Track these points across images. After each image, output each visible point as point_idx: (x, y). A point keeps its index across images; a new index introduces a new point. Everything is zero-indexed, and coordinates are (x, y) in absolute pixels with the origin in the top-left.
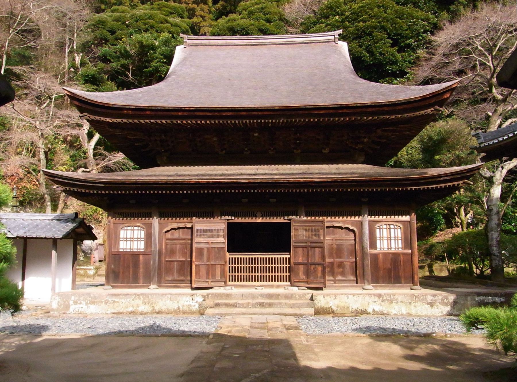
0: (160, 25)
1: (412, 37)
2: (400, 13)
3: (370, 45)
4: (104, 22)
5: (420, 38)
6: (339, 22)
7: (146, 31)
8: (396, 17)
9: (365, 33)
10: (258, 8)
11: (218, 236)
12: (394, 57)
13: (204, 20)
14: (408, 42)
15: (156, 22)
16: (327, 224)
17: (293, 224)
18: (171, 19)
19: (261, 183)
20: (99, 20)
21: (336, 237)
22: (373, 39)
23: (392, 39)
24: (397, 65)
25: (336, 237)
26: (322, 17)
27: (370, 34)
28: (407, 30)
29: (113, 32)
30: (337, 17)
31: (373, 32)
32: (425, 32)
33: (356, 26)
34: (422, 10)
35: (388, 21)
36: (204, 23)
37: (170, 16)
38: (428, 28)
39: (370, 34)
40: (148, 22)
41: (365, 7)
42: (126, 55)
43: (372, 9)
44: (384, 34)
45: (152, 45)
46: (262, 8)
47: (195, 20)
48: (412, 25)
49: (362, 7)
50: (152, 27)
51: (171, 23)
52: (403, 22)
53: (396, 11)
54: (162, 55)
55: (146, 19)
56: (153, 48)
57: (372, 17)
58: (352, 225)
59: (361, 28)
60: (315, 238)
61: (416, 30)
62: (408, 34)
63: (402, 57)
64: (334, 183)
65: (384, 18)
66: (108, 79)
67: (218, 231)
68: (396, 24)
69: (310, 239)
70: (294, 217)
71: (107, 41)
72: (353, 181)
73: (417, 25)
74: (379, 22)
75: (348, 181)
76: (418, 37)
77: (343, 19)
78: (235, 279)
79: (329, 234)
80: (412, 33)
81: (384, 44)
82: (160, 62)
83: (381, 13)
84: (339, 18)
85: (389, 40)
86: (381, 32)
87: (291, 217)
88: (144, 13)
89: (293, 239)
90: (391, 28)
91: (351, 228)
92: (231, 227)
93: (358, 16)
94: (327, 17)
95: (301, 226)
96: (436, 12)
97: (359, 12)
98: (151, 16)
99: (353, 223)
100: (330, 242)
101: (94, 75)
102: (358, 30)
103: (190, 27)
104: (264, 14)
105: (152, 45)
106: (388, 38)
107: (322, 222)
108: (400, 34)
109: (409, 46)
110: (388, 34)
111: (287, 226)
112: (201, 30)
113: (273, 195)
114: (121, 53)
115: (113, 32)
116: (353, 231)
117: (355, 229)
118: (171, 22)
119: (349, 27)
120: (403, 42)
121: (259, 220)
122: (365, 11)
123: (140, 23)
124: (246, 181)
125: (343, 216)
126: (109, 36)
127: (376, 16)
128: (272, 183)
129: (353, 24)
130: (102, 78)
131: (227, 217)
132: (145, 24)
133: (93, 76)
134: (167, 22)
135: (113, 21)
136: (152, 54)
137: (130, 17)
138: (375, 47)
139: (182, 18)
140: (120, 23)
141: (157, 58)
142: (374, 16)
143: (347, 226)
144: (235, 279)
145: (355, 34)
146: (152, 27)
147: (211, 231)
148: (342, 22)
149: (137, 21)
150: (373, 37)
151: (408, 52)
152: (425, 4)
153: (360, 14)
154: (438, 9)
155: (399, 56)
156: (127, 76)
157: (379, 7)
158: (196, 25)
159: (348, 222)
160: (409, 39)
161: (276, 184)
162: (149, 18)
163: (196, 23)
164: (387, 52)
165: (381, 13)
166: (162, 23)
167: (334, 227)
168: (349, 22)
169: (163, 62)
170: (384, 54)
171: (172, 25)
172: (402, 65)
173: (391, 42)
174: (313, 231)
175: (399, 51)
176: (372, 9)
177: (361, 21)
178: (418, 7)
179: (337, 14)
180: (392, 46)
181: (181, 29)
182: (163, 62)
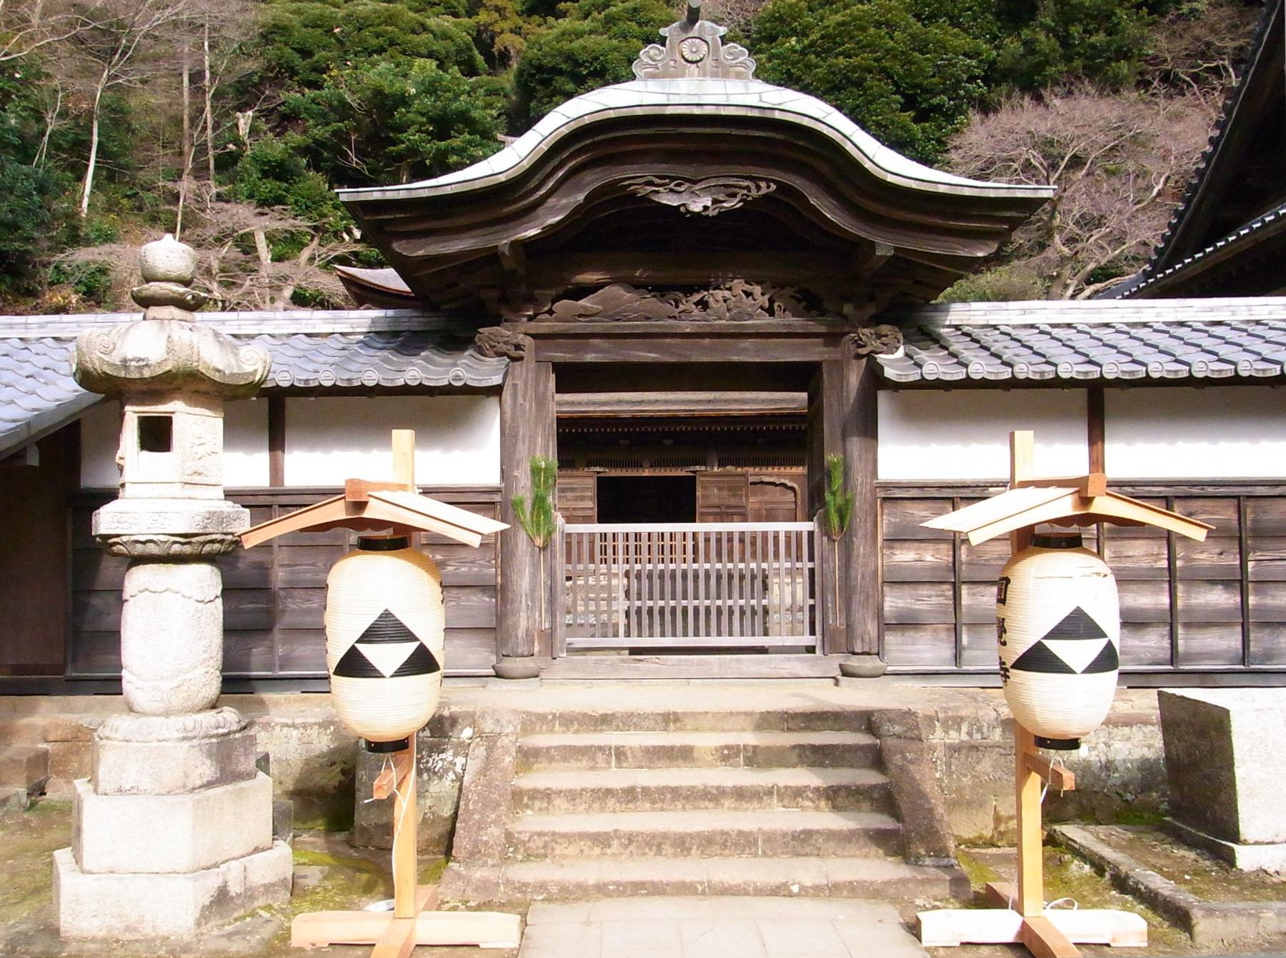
0: (410, 37)
1: (943, 92)
2: (922, 40)
3: (858, 106)
4: (285, 28)
5: (962, 92)
6: (796, 51)
7: (381, 50)
8: (913, 49)
9: (849, 80)
10: (626, 11)
11: (583, 498)
12: (908, 131)
13: (504, 18)
14: (935, 101)
15: (401, 29)
16: (751, 479)
17: (699, 479)
18: (432, 22)
19: (651, 418)
20: (274, 25)
21: (766, 498)
22: (865, 94)
23: (903, 95)
24: (913, 147)
25: (766, 498)
26: (763, 39)
27: (859, 84)
28: (933, 76)
29: (306, 53)
30: (793, 41)
31: (865, 80)
32: (972, 79)
33: (830, 66)
34: (965, 30)
35: (895, 57)
36: (506, 25)
37: (429, 12)
38: (977, 72)
39: (859, 84)
40: (386, 32)
41: (849, 23)
42: (343, 110)
43: (864, 29)
44: (887, 84)
45: (403, 94)
46: (635, 10)
47: (483, 17)
48: (945, 66)
49: (843, 24)
50: (392, 43)
51: (432, 32)
52: (927, 59)
53: (913, 37)
54: (423, 115)
55: (379, 25)
56: (403, 100)
57: (863, 47)
58: (791, 480)
59: (840, 70)
60: (732, 501)
61: (952, 75)
62: (936, 84)
63: (924, 130)
64: (761, 418)
65: (888, 51)
66: (308, 166)
67: (584, 490)
68: (911, 63)
69: (726, 502)
70: (703, 468)
71: (293, 72)
72: (790, 415)
73: (954, 65)
74: (877, 60)
75: (782, 415)
76: (955, 91)
77: (804, 48)
78: (753, 544)
79: (754, 495)
80: (944, 84)
81: (888, 104)
82: (419, 131)
83: (881, 38)
84: (798, 42)
85: (898, 97)
86: (880, 80)
87: (698, 468)
88: (375, 12)
89: (699, 502)
90: (901, 71)
91: (789, 484)
92: (603, 483)
93: (835, 43)
94: (772, 39)
95: (712, 482)
96: (995, 37)
97: (836, 36)
98: (390, 17)
99: (792, 477)
100: (757, 506)
101: (282, 161)
102: (834, 73)
103: (474, 39)
104: (640, 24)
105: (403, 94)
106: (895, 93)
107: (745, 475)
108: (919, 86)
109: (938, 108)
110: (895, 83)
111: (690, 482)
112: (497, 40)
113: (668, 435)
114: (330, 106)
115: (306, 53)
116: (793, 489)
117: (796, 486)
118: (434, 28)
119: (816, 67)
120: (926, 100)
121: (647, 473)
122: (849, 32)
123: (366, 33)
124: (628, 415)
125: (780, 465)
126: (297, 60)
127: (870, 47)
128: (668, 418)
129: (824, 60)
130: (297, 165)
131: (598, 469)
132: (378, 36)
133: (281, 164)
134: (425, 28)
135: (306, 26)
136: (403, 115)
137: (344, 18)
138: (869, 111)
139: (456, 15)
140: (320, 31)
141: (413, 123)
142: (868, 46)
143: (783, 481)
144: (753, 544)
145: (828, 82)
146: (392, 43)
147: (572, 490)
148: (803, 52)
149: (360, 29)
150: (865, 91)
151: (935, 120)
152: (975, 19)
153: (838, 39)
154: (999, 29)
155: (916, 128)
156: (346, 156)
157: (878, 25)
158: (486, 30)
159: (785, 476)
160: (939, 94)
161: (674, 420)
162: (386, 23)
163: (486, 26)
164: (893, 122)
165: (881, 38)
166: (414, 32)
167: (762, 483)
168: (817, 56)
169: (427, 132)
170: (886, 127)
171: (435, 35)
172: (924, 148)
173: (902, 100)
174: (730, 489)
175: (916, 120)
176: (864, 29)
177: (841, 54)
178: (958, 25)
179: (794, 32)
180: (904, 109)
181: (455, 45)
182: (427, 132)
